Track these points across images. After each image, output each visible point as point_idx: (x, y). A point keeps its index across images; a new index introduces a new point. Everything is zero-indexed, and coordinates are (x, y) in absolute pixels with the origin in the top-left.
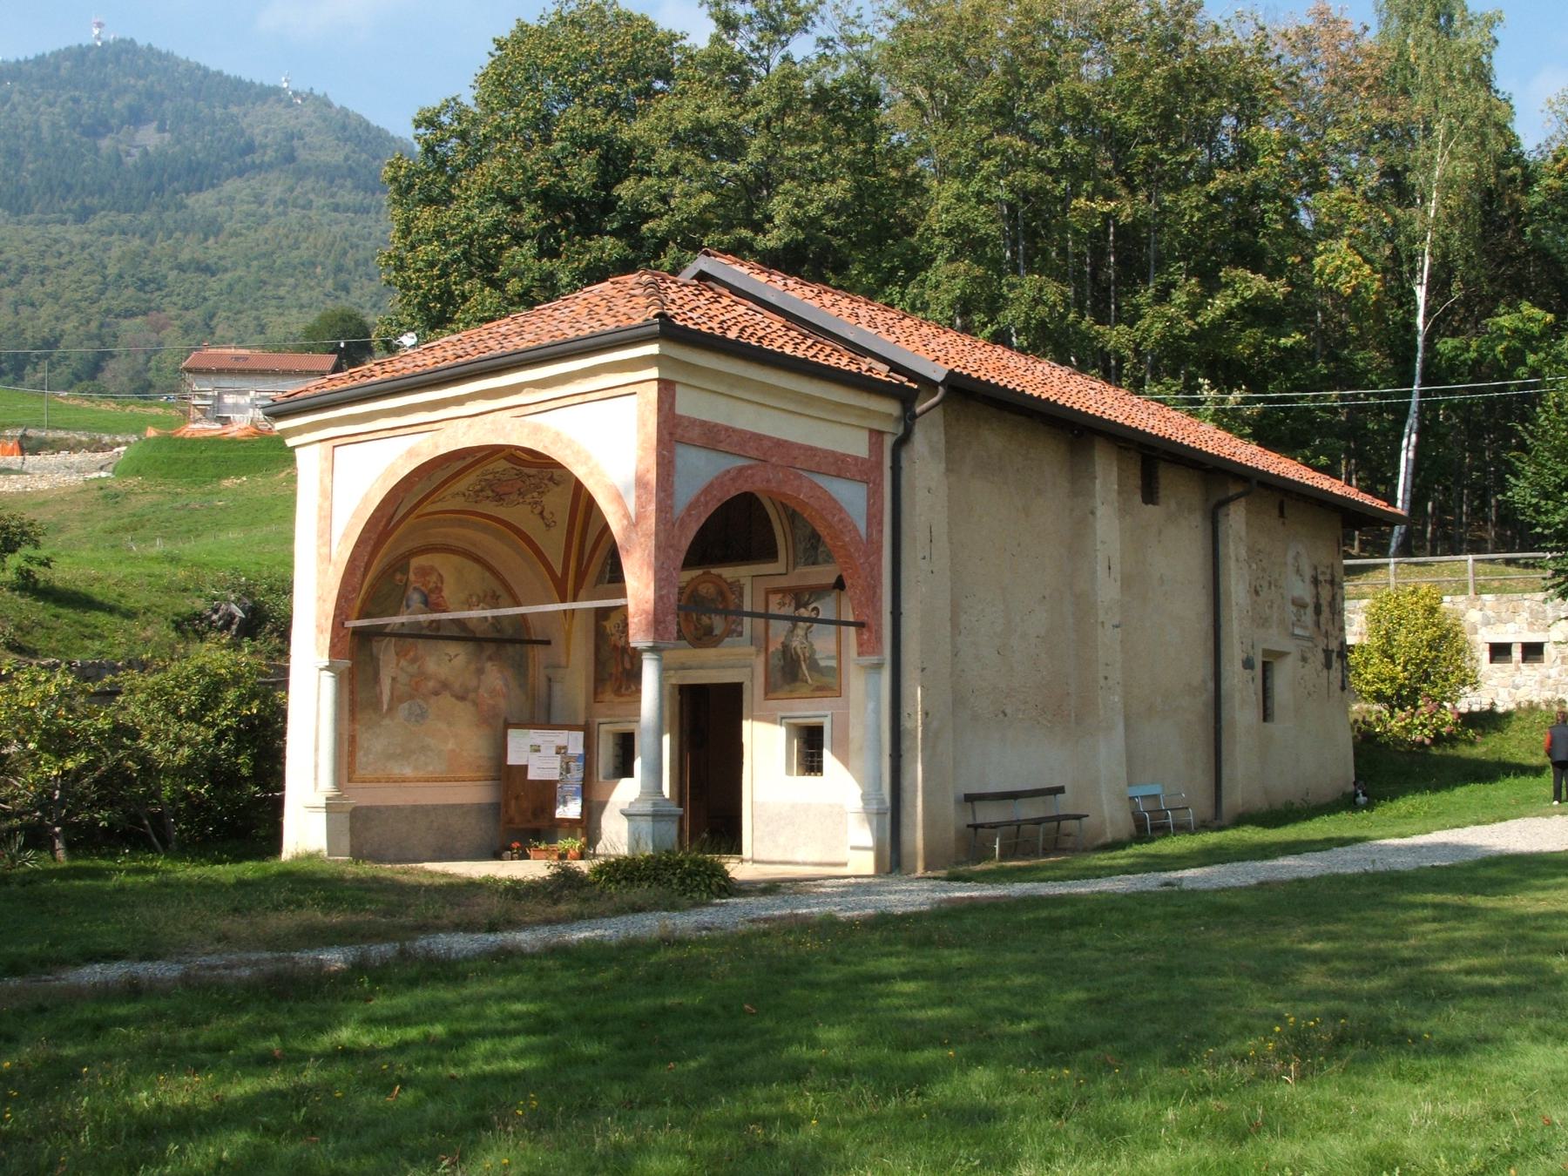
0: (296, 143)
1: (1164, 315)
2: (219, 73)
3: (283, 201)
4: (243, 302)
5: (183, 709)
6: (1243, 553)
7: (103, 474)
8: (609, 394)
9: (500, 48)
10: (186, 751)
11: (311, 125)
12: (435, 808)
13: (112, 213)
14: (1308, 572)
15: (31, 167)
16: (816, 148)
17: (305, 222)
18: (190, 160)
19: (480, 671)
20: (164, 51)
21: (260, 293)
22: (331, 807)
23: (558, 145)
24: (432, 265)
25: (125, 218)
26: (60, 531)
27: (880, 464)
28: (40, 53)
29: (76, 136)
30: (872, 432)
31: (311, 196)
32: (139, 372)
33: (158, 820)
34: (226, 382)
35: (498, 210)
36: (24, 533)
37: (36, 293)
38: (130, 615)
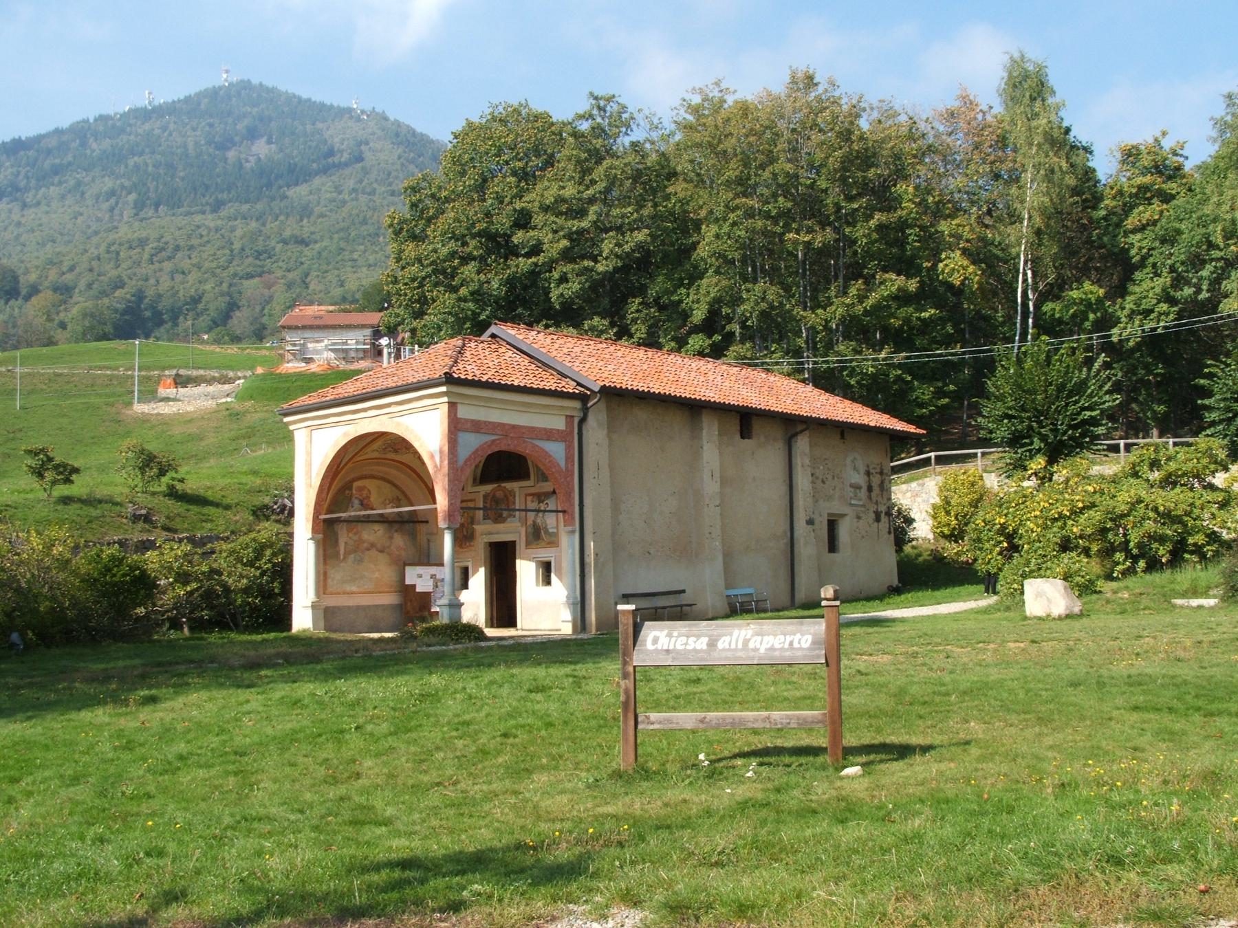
0: (363, 147)
1: (843, 303)
2: (309, 100)
3: (354, 190)
4: (328, 264)
5: (245, 560)
6: (807, 462)
7: (229, 400)
8: (428, 409)
9: (456, 137)
10: (245, 581)
11: (373, 134)
12: (369, 606)
13: (237, 204)
14: (862, 469)
15: (182, 174)
16: (629, 209)
17: (371, 204)
18: (290, 164)
19: (391, 538)
20: (270, 86)
21: (339, 258)
22: (314, 607)
23: (490, 201)
24: (413, 280)
25: (245, 207)
26: (201, 439)
27: (572, 432)
28: (187, 94)
29: (211, 150)
30: (567, 416)
31: (375, 185)
32: (256, 319)
33: (233, 616)
34: (308, 334)
35: (452, 245)
36: (170, 465)
37: (186, 264)
38: (227, 507)
